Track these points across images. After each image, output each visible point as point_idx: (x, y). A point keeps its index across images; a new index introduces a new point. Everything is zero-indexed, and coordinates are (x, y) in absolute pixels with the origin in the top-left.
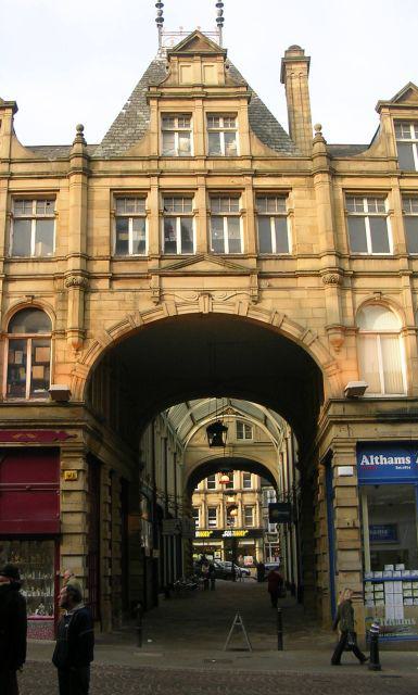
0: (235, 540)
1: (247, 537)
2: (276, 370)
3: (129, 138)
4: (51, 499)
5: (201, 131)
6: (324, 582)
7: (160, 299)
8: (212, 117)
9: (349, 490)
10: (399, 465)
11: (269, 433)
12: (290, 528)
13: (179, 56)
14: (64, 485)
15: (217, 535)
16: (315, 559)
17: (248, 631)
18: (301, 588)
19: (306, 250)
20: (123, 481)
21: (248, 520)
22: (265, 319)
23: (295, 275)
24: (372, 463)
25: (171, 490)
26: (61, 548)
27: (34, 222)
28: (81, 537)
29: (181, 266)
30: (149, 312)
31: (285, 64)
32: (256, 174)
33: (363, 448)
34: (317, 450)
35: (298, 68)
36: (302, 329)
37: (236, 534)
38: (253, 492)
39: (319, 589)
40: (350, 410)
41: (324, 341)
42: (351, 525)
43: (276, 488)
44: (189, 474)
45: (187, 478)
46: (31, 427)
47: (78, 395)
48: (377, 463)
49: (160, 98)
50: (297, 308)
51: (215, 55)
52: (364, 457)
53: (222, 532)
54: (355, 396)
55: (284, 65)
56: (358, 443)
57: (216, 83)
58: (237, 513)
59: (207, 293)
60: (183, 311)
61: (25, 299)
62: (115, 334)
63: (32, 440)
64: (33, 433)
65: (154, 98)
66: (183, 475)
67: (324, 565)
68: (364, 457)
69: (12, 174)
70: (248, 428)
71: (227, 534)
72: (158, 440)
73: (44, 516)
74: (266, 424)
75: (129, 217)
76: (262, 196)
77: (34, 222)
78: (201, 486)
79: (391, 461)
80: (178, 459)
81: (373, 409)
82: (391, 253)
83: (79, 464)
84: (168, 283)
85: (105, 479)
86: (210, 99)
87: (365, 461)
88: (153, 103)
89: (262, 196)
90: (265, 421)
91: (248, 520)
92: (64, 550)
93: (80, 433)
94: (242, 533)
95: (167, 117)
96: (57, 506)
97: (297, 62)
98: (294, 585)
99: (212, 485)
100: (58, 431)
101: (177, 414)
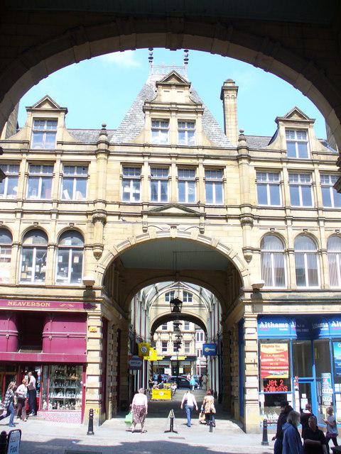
0: (178, 361)
2: (220, 276)
3: (131, 131)
4: (81, 342)
6: (235, 393)
8: (181, 122)
11: (199, 301)
12: (215, 359)
13: (163, 85)
14: (89, 335)
16: (231, 379)
17: (181, 403)
20: (119, 331)
21: (187, 350)
22: (207, 242)
25: (143, 334)
27: (75, 180)
28: (98, 352)
29: (161, 210)
30: (141, 236)
31: (223, 90)
32: (62, 153)
35: (231, 93)
37: (180, 358)
39: (232, 397)
42: (253, 362)
43: (205, 330)
46: (70, 300)
49: (151, 110)
50: (230, 240)
51: (184, 86)
53: (171, 357)
55: (223, 91)
57: (184, 102)
59: (174, 226)
61: (68, 225)
62: (120, 249)
63: (72, 308)
64: (72, 304)
65: (147, 110)
69: (243, 193)
70: (190, 295)
72: (137, 303)
73: (78, 352)
75: (336, 253)
76: (209, 170)
77: (75, 180)
82: (313, 207)
83: (99, 323)
85: (111, 331)
86: (180, 112)
88: (147, 113)
89: (209, 170)
91: (187, 350)
92: (88, 372)
94: (183, 358)
95: (155, 121)
96: (85, 346)
97: (230, 90)
98: (216, 393)
99: (165, 328)
101: (148, 291)
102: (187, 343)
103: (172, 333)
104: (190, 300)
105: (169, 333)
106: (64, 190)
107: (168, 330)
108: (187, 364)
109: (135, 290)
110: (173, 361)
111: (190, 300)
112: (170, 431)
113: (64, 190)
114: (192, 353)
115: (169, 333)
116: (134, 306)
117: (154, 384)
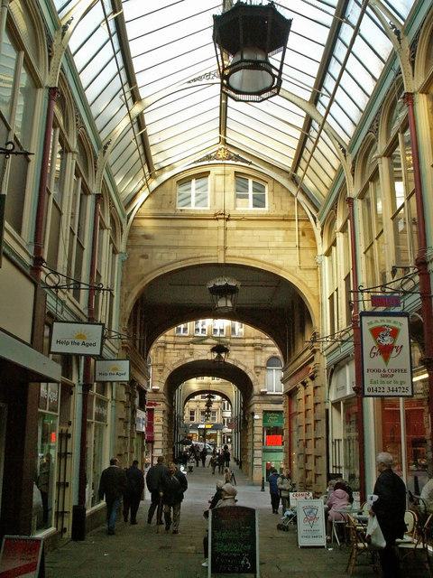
0: (205, 430)
5: (222, 168)
7: (192, 354)
18: (241, 462)
19: (249, 335)
23: (245, 345)
25: (169, 154)
26: (420, 302)
33: (265, 412)
36: (246, 367)
40: (262, 398)
41: (253, 371)
47: (161, 390)
54: (263, 394)
60: (201, 358)
67: (250, 453)
81: (270, 398)
84: (195, 347)
90: (377, 321)
92: (155, 447)
93: (161, 403)
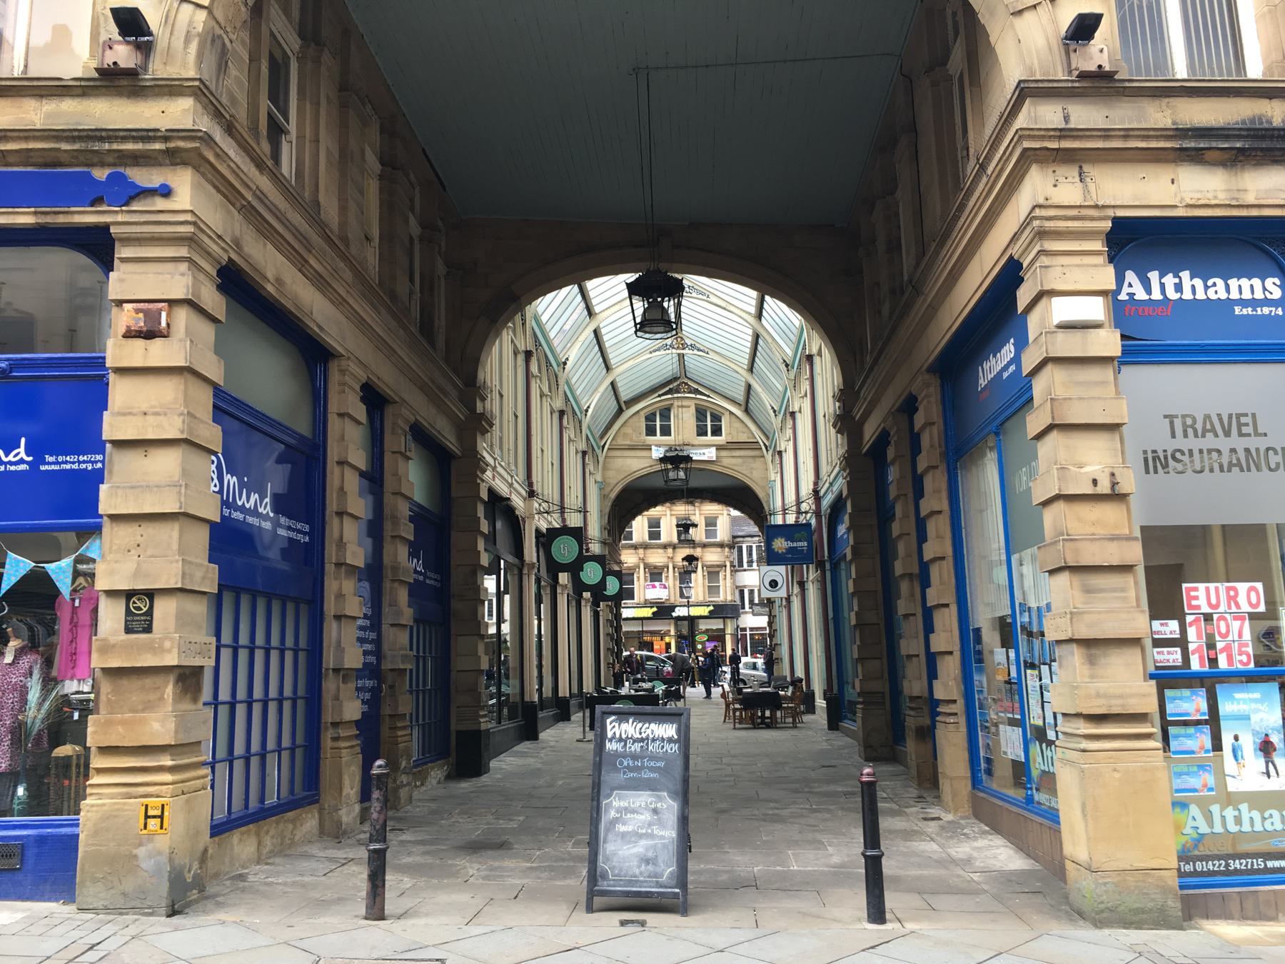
0: (692, 620)
1: (712, 615)
9: (1094, 374)
10: (1243, 303)
15: (663, 611)
21: (713, 590)
24: (1156, 295)
33: (1134, 240)
34: (934, 309)
37: (695, 612)
38: (721, 545)
42: (1104, 488)
44: (613, 495)
45: (609, 504)
48: (1172, 295)
52: (1130, 276)
53: (673, 608)
56: (1116, 221)
58: (698, 579)
66: (603, 497)
68: (1130, 276)
70: (716, 418)
71: (680, 612)
74: (747, 411)
78: (639, 527)
79: (1218, 290)
80: (590, 467)
87: (1134, 287)
91: (713, 590)
94: (704, 611)
100: (101, 174)
102: (713, 573)
103: (674, 547)
104: (717, 431)
105: (665, 547)
106: (230, 258)
107: (664, 538)
108: (716, 624)
109: (509, 301)
110: (679, 618)
111: (717, 431)
112: (620, 411)
113: (230, 258)
114: (726, 594)
115: (665, 547)
116: (500, 363)
117: (491, 491)
